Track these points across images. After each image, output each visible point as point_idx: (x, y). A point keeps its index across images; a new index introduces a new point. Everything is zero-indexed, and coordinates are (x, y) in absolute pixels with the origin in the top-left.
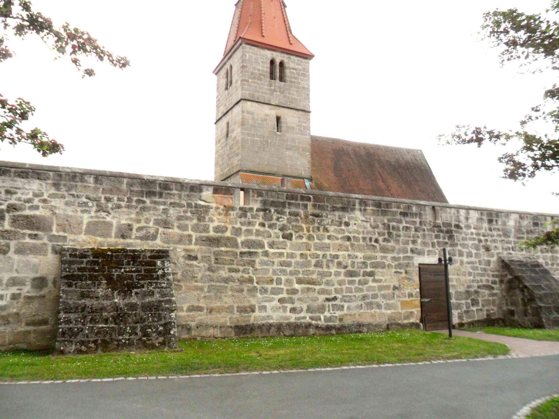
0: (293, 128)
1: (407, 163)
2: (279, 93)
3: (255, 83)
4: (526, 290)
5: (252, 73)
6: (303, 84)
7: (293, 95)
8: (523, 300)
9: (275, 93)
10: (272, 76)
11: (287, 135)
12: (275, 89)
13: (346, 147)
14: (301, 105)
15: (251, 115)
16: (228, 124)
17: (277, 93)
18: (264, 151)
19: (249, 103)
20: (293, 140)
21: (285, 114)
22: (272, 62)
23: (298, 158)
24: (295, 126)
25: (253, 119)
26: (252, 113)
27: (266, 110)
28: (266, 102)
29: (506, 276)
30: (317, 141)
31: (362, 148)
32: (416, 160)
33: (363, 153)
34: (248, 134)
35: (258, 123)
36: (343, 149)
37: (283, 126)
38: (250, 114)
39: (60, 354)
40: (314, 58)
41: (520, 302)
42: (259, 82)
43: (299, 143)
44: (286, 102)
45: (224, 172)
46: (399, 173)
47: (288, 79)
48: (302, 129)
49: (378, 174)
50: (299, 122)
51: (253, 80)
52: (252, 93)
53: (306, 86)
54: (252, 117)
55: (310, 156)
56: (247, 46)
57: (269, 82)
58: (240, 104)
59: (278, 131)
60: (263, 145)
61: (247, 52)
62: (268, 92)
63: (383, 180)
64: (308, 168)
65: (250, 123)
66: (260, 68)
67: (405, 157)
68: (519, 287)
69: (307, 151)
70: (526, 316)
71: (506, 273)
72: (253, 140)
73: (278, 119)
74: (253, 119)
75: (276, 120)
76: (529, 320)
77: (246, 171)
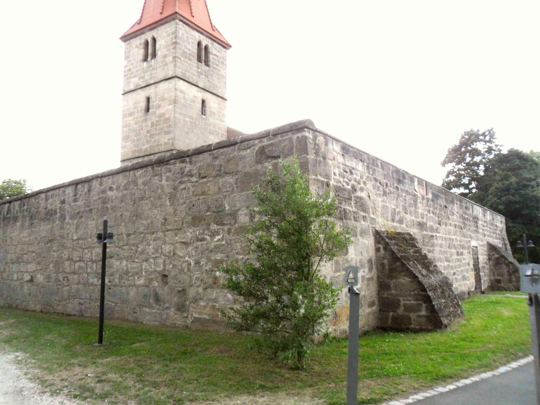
3: (185, 61)
4: (510, 265)
5: (184, 51)
6: (222, 72)
7: (214, 81)
8: (508, 272)
10: (199, 60)
11: (210, 120)
12: (201, 72)
16: (148, 99)
19: (182, 82)
21: (209, 98)
22: (199, 44)
25: (184, 98)
28: (195, 83)
29: (494, 255)
39: (491, 283)
40: (120, 36)
41: (506, 273)
42: (189, 62)
43: (219, 128)
45: (141, 149)
47: (211, 64)
50: (219, 108)
51: (185, 59)
53: (224, 75)
56: (180, 23)
57: (197, 64)
58: (173, 81)
61: (180, 29)
62: (196, 74)
66: (190, 47)
68: (504, 263)
70: (511, 283)
71: (493, 253)
73: (203, 102)
76: (513, 286)
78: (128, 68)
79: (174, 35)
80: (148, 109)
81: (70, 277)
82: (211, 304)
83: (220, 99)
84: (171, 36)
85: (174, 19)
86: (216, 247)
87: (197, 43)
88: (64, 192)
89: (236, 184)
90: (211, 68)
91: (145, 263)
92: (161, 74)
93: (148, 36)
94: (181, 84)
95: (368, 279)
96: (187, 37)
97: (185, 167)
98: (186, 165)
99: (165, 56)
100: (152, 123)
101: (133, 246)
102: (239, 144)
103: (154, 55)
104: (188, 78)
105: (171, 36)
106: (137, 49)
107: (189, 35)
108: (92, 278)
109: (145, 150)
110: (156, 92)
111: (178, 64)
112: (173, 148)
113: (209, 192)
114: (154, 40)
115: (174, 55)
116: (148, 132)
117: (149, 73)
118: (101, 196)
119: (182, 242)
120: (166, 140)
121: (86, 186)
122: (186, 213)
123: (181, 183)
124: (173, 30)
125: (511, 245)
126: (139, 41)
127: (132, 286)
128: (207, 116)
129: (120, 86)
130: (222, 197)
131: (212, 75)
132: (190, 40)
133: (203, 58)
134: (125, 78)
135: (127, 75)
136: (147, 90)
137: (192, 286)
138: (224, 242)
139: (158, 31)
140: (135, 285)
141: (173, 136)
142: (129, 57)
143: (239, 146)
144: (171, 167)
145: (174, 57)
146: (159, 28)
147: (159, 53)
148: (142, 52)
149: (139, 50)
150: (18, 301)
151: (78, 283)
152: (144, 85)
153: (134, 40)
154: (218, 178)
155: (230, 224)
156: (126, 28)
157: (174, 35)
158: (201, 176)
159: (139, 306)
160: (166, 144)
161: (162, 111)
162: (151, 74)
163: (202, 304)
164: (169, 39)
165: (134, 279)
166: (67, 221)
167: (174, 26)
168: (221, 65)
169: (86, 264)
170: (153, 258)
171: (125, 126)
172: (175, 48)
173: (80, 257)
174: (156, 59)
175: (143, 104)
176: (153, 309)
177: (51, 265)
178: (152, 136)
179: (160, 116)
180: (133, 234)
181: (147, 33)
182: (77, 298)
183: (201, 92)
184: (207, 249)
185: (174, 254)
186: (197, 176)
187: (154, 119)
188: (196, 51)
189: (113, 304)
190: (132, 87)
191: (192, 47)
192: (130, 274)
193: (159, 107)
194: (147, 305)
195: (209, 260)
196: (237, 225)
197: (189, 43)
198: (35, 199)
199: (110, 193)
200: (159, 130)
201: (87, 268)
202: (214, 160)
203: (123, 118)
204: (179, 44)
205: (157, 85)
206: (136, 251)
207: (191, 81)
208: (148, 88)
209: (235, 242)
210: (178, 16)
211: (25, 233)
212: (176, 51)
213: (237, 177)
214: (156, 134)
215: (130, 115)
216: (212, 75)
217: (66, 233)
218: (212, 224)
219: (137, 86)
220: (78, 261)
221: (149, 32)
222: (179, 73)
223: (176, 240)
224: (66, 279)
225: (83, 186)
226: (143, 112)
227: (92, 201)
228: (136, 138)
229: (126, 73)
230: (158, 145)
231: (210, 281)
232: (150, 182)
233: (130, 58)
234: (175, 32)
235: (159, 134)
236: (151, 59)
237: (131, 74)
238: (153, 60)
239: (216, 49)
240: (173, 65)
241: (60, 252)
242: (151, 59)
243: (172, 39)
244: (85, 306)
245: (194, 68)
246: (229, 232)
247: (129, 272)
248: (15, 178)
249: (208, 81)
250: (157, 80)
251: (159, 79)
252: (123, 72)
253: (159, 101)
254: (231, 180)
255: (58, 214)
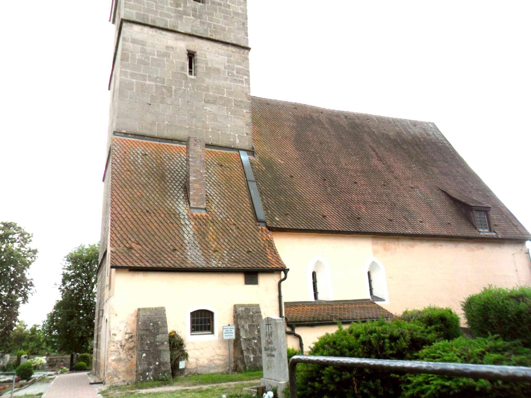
0: (218, 70)
1: (414, 137)
2: (192, 17)
7: (218, 22)
9: (184, 17)
11: (207, 80)
13: (317, 115)
14: (232, 37)
15: (140, 46)
17: (189, 17)
18: (162, 103)
19: (136, 28)
20: (219, 89)
23: (227, 117)
24: (222, 68)
25: (143, 51)
26: (143, 43)
27: (169, 39)
30: (268, 104)
31: (342, 117)
32: (429, 135)
33: (344, 122)
34: (133, 75)
35: (153, 59)
36: (311, 117)
37: (200, 66)
38: (138, 43)
43: (230, 93)
44: (206, 30)
46: (402, 148)
48: (235, 72)
49: (370, 149)
50: (229, 61)
52: (142, 12)
54: (141, 48)
55: (250, 115)
59: (190, 72)
60: (162, 93)
62: (173, 15)
63: (379, 157)
64: (247, 134)
65: (137, 57)
67: (410, 130)
69: (245, 108)
72: (143, 85)
73: (191, 56)
74: (143, 51)
75: (186, 56)
77: (126, 134)
95: (130, 349)
125: (214, 383)
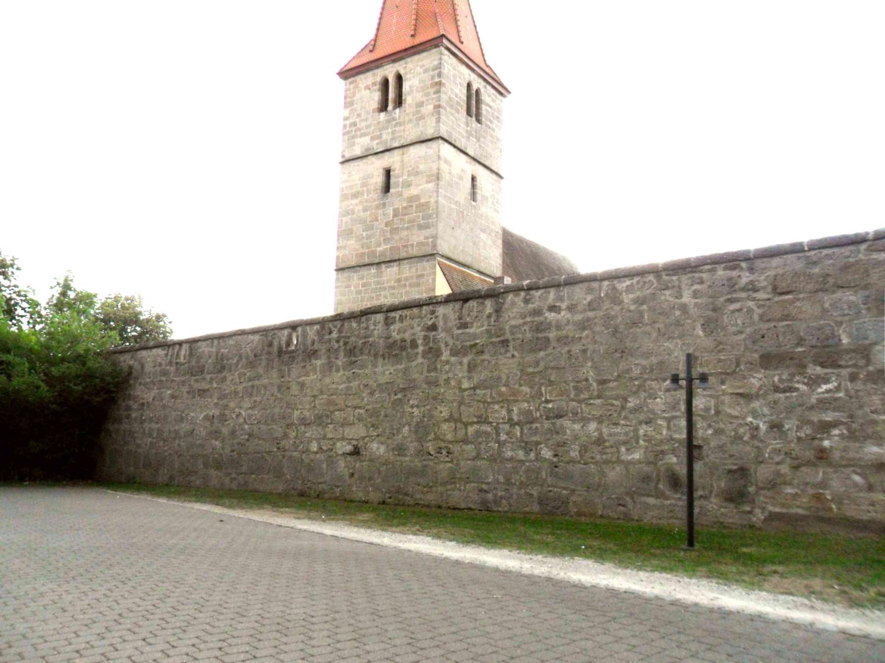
5: (450, 98)
10: (469, 113)
16: (388, 173)
19: (447, 145)
21: (483, 176)
22: (469, 85)
28: (463, 148)
40: (338, 70)
42: (456, 115)
47: (484, 120)
50: (493, 190)
56: (446, 52)
58: (433, 145)
62: (465, 135)
73: (473, 179)
78: (351, 121)
79: (436, 72)
80: (387, 188)
81: (456, 448)
82: (811, 491)
83: (494, 176)
84: (431, 73)
85: (437, 46)
86: (821, 401)
87: (466, 85)
88: (433, 312)
89: (865, 304)
90: (484, 126)
91: (644, 426)
92: (412, 133)
93: (389, 71)
94: (445, 149)
96: (454, 75)
97: (739, 276)
98: (742, 274)
99: (420, 104)
100: (394, 210)
101: (615, 399)
102: (869, 243)
103: (399, 102)
104: (455, 141)
105: (431, 73)
106: (368, 91)
107: (456, 73)
108: (512, 450)
109: (382, 253)
110: (402, 161)
111: (443, 118)
112: (435, 252)
113: (803, 316)
114: (399, 79)
115: (437, 103)
116: (387, 225)
117: (390, 130)
118: (528, 319)
119: (737, 394)
120: (422, 239)
121: (489, 306)
122: (746, 348)
123: (731, 301)
124: (436, 63)
126: (373, 78)
127: (614, 463)
128: (478, 202)
129: (337, 148)
130: (832, 324)
131: (485, 138)
132: (458, 81)
133: (474, 109)
134: (346, 137)
135: (348, 132)
136: (386, 158)
137: (762, 462)
138: (841, 395)
139: (406, 63)
140: (619, 461)
141: (434, 233)
142: (353, 104)
143: (870, 246)
144: (704, 275)
145: (438, 107)
146: (409, 60)
147: (409, 99)
148: (377, 96)
149: (371, 93)
150: (324, 486)
151: (477, 457)
152: (381, 150)
153: (362, 76)
154: (820, 294)
155: (855, 366)
156: (346, 56)
157: (436, 72)
158: (779, 290)
159: (631, 494)
160: (420, 244)
161: (413, 191)
162: (393, 132)
163: (789, 490)
164: (426, 77)
165: (618, 452)
166: (443, 358)
167: (438, 57)
168: (495, 121)
169: (497, 429)
170: (665, 418)
171: (346, 213)
172: (438, 92)
173: (479, 417)
174: (403, 109)
175: (379, 180)
176: (667, 498)
177: (407, 428)
178: (395, 230)
179: (411, 199)
180: (615, 381)
181: (385, 67)
182: (471, 482)
183: (470, 163)
184: (801, 405)
185: (718, 413)
186: (770, 288)
187: (399, 204)
188: (465, 99)
189: (564, 492)
190: (358, 151)
191: (461, 91)
192: (607, 444)
193: (408, 185)
194: (653, 493)
195: (804, 422)
196: (871, 368)
197: (456, 83)
198: (359, 323)
199: (551, 316)
200: (408, 222)
201: (498, 434)
202: (810, 266)
203: (341, 201)
204: (444, 84)
205: (405, 149)
206: (623, 408)
207: (457, 144)
208: (387, 153)
209: (869, 394)
210: (445, 41)
211: (338, 376)
212: (439, 97)
213: (867, 293)
214: (403, 229)
215: (355, 196)
216: (485, 138)
217: (445, 377)
218: (811, 365)
219: (367, 150)
220: (473, 423)
221: (391, 65)
222: (444, 131)
223: (723, 391)
224: (444, 452)
225: (483, 303)
226: (379, 191)
227: (507, 327)
228: (364, 234)
229: (348, 129)
230: (404, 246)
231: (810, 454)
232: (654, 299)
233: (355, 106)
234: (439, 67)
235: (408, 228)
236: (394, 108)
237: (356, 131)
238: (397, 110)
239: (489, 96)
240: (434, 119)
241: (428, 407)
242: (394, 108)
243: (433, 77)
244: (495, 495)
245: (463, 125)
246: (853, 378)
247: (605, 441)
248: (125, 292)
249: (480, 146)
250: (403, 142)
251: (408, 141)
252: (341, 127)
253: (409, 176)
254: (853, 298)
255: (421, 349)
